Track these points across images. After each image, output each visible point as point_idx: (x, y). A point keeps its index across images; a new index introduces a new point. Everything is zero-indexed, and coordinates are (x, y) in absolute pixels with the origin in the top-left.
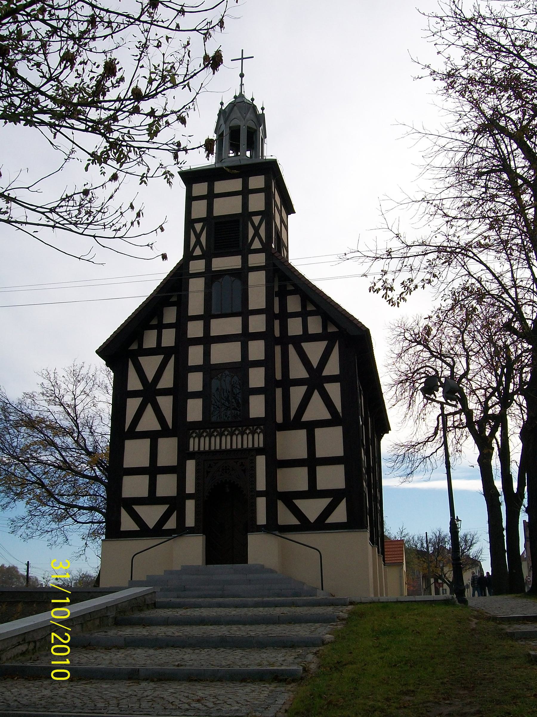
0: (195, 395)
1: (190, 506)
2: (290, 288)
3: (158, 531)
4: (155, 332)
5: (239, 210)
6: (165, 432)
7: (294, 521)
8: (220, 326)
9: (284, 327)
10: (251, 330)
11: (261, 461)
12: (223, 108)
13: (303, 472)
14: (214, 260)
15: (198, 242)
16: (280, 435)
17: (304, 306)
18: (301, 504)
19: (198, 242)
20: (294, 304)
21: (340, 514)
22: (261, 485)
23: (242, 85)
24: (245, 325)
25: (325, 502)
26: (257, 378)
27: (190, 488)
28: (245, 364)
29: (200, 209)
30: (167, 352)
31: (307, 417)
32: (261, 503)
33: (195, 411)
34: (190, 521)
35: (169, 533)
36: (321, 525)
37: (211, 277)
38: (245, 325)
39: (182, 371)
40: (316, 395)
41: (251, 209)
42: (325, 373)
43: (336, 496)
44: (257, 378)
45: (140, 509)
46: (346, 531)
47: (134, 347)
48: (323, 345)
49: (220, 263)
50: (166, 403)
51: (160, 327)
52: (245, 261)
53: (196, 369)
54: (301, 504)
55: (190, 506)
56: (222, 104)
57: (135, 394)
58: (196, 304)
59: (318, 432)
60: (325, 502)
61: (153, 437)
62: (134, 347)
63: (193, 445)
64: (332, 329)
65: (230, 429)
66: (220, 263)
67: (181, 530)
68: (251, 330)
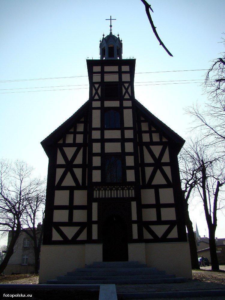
0: (97, 168)
1: (95, 227)
2: (143, 119)
3: (74, 241)
4: (72, 136)
5: (117, 80)
6: (78, 187)
7: (150, 237)
8: (109, 134)
9: (141, 138)
10: (126, 137)
11: (134, 204)
12: (104, 37)
13: (154, 211)
14: (105, 102)
15: (97, 93)
16: (143, 191)
17: (150, 128)
18: (153, 228)
19: (97, 93)
20: (145, 127)
21: (174, 234)
22: (134, 217)
23: (111, 30)
24: (123, 134)
25: (166, 227)
26: (130, 161)
27: (95, 218)
28: (123, 154)
29: (97, 78)
30: (79, 146)
31: (155, 182)
32: (135, 227)
33: (97, 176)
34: (95, 236)
35: (82, 242)
36: (164, 239)
37: (104, 110)
38: (123, 134)
39: (89, 155)
40: (158, 172)
41: (124, 80)
42: (163, 161)
43: (171, 224)
44: (130, 161)
45: (63, 229)
46: (183, 242)
47: (61, 142)
48: (161, 147)
49: (108, 104)
50: (78, 172)
51: (75, 133)
52: (121, 104)
53: (97, 155)
54: (153, 228)
55: (95, 227)
56: (104, 35)
57: (61, 166)
58: (96, 122)
59: (161, 191)
60: (166, 227)
61: (71, 189)
62: (61, 142)
63: (96, 194)
64: (164, 140)
65: (116, 187)
66: (108, 104)
67: (89, 240)
68: (126, 137)
